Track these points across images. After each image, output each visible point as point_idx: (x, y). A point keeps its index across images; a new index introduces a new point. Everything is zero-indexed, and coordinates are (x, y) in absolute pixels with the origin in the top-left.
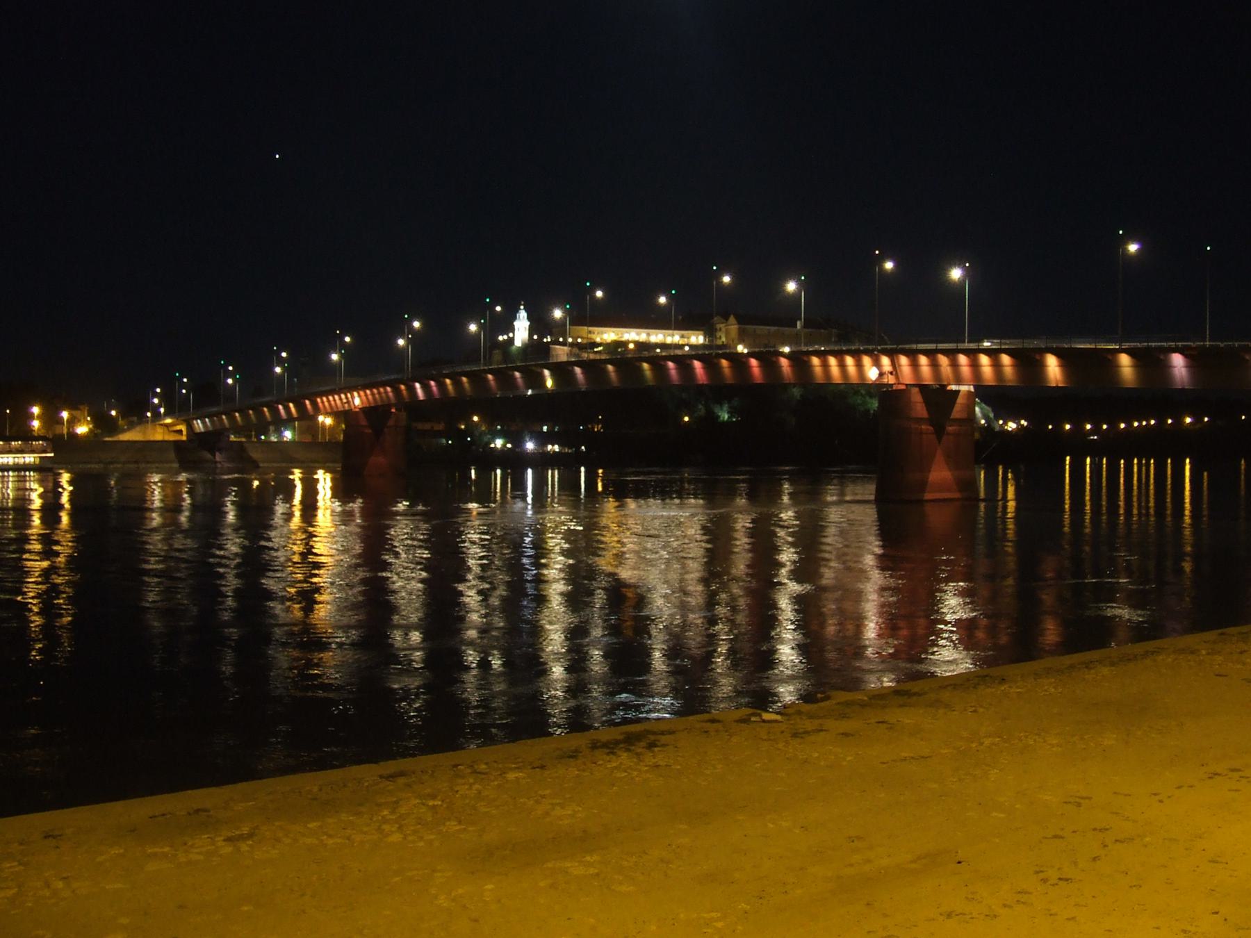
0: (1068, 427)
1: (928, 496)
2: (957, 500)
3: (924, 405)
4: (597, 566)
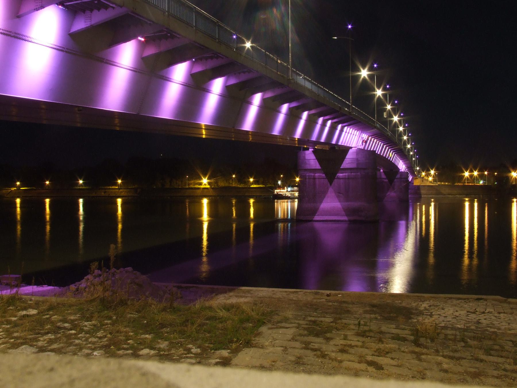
0: (496, 174)
1: (316, 218)
2: (345, 221)
3: (316, 160)
4: (243, 52)
